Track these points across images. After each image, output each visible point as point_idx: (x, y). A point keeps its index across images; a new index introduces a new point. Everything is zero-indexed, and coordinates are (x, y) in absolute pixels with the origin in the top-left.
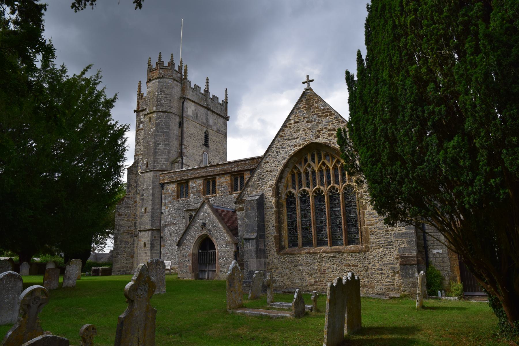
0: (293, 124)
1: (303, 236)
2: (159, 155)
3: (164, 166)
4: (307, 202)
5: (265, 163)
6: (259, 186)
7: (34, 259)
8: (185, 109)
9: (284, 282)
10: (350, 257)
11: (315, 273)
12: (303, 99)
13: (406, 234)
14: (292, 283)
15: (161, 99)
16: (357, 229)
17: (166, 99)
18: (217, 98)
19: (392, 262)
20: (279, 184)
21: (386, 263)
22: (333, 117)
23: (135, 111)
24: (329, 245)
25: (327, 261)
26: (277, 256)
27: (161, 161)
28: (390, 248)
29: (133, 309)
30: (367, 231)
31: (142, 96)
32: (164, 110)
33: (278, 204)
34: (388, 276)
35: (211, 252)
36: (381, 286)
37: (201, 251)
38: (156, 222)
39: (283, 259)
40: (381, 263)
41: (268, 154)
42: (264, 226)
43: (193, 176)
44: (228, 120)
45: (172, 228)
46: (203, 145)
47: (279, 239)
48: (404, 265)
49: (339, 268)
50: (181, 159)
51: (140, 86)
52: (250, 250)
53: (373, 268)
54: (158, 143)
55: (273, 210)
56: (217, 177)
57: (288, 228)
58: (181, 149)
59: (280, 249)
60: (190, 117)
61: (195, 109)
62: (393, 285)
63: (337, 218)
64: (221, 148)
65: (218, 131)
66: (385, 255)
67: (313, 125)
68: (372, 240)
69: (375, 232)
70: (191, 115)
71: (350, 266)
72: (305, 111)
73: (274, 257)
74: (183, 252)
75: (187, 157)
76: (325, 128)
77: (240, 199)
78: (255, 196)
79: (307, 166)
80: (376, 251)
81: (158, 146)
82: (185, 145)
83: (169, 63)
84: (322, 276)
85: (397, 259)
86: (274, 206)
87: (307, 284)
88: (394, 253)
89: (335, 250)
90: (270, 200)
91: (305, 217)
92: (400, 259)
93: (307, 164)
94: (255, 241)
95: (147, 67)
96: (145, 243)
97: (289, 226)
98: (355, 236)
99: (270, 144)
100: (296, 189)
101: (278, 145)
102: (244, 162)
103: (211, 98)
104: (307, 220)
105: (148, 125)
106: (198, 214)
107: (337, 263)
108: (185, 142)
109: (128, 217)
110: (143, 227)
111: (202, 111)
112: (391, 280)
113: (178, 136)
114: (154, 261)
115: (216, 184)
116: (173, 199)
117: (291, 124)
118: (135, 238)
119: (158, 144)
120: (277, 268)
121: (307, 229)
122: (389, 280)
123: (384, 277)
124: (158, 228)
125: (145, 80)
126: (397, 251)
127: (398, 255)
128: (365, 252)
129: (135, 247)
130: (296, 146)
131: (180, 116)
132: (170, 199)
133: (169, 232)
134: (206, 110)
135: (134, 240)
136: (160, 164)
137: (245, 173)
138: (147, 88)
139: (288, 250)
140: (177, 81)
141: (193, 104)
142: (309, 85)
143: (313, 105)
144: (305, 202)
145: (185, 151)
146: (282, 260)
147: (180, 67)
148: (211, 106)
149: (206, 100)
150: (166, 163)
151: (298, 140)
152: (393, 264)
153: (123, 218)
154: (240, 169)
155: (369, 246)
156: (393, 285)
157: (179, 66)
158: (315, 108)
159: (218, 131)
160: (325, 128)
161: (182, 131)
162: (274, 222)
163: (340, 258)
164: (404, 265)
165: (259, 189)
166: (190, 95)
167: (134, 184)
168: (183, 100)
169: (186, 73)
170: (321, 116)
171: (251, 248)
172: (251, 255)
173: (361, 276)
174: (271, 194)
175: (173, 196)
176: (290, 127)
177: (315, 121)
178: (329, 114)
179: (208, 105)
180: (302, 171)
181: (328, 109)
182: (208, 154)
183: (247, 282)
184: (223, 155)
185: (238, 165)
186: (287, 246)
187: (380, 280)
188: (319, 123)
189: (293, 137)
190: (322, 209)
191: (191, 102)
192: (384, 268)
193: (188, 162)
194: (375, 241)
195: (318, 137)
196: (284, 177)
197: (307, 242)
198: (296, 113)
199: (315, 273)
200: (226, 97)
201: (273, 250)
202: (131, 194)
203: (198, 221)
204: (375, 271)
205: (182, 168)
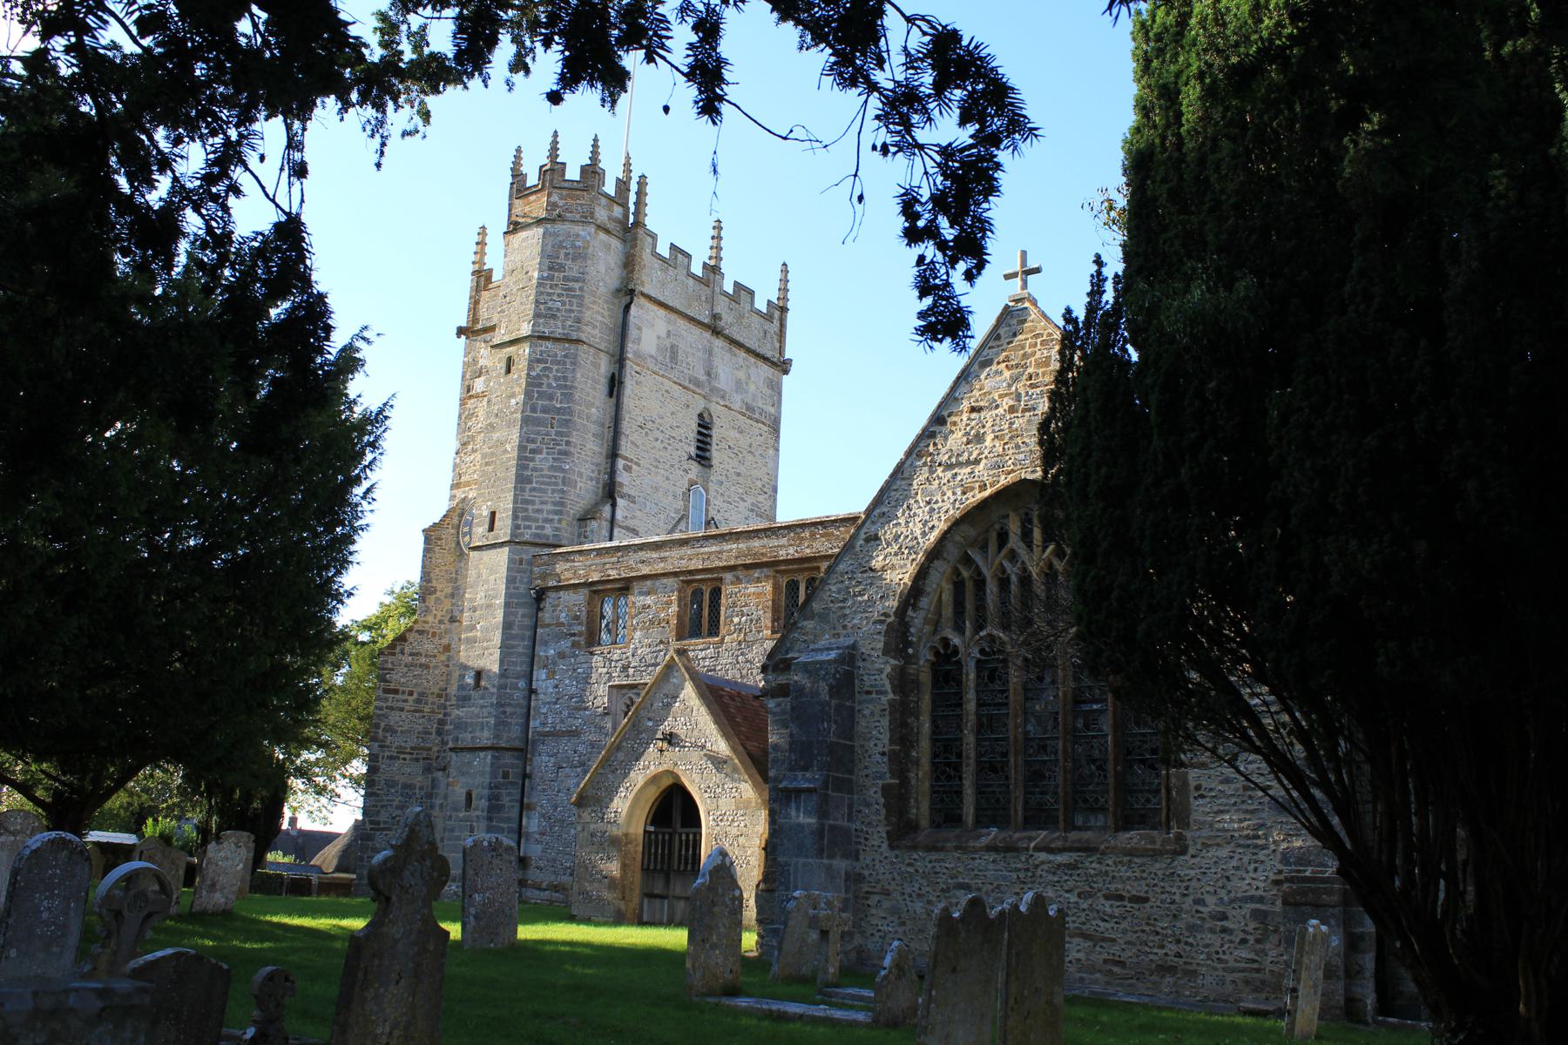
1: (980, 792)
2: (534, 489)
3: (548, 530)
4: (1000, 679)
8: (632, 332)
10: (1123, 869)
12: (1002, 331)
15: (549, 294)
16: (1158, 776)
17: (567, 296)
18: (751, 293)
19: (1260, 892)
20: (910, 613)
21: (1239, 895)
23: (461, 331)
24: (1061, 825)
25: (1051, 877)
27: (538, 511)
28: (1256, 846)
29: (387, 920)
31: (489, 279)
32: (559, 332)
33: (903, 682)
34: (1244, 941)
36: (1221, 973)
38: (513, 721)
39: (909, 865)
40: (1223, 893)
41: (877, 512)
42: (851, 749)
43: (646, 570)
44: (786, 372)
45: (565, 746)
46: (690, 458)
47: (897, 799)
48: (1297, 904)
49: (1085, 906)
50: (607, 508)
51: (481, 244)
53: (1197, 911)
54: (532, 446)
55: (884, 699)
56: (728, 576)
57: (933, 764)
58: (612, 473)
59: (902, 832)
60: (649, 360)
61: (669, 333)
62: (1258, 971)
63: (1093, 737)
64: (754, 473)
65: (749, 411)
66: (1237, 868)
69: (1211, 790)
70: (653, 353)
75: (631, 499)
78: (828, 649)
79: (1005, 557)
80: (1210, 855)
81: (533, 460)
82: (626, 458)
83: (584, 169)
86: (888, 687)
89: (1077, 845)
92: (1286, 886)
93: (1004, 552)
94: (815, 797)
95: (510, 180)
96: (469, 795)
97: (935, 755)
98: (1148, 801)
99: (886, 477)
100: (968, 633)
103: (726, 294)
104: (997, 739)
105: (500, 384)
108: (625, 448)
109: (418, 701)
110: (466, 738)
111: (693, 338)
112: (1252, 956)
113: (603, 425)
114: (485, 844)
115: (723, 601)
116: (574, 645)
118: (440, 774)
119: (533, 451)
120: (887, 893)
122: (1245, 954)
123: (1231, 942)
124: (517, 744)
125: (499, 224)
127: (1280, 872)
129: (437, 808)
131: (613, 356)
132: (565, 644)
133: (552, 760)
134: (707, 335)
135: (433, 780)
136: (536, 520)
138: (505, 256)
140: (607, 231)
141: (662, 312)
142: (1025, 285)
143: (1034, 354)
144: (992, 679)
145: (623, 477)
147: (623, 185)
148: (727, 319)
149: (711, 301)
150: (556, 517)
152: (1261, 900)
153: (400, 704)
154: (808, 551)
155: (1188, 834)
156: (1258, 971)
157: (618, 180)
158: (1038, 365)
159: (749, 411)
161: (618, 407)
162: (886, 738)
163: (1092, 872)
164: (1297, 904)
166: (650, 280)
167: (443, 588)
168: (628, 298)
169: (640, 203)
173: (1157, 933)
174: (881, 645)
175: (574, 635)
179: (716, 317)
180: (987, 573)
182: (707, 491)
184: (761, 498)
185: (802, 539)
186: (924, 823)
187: (1217, 953)
191: (655, 308)
192: (1234, 912)
193: (634, 517)
196: (928, 589)
197: (993, 814)
200: (784, 290)
201: (878, 837)
202: (430, 619)
204: (1203, 919)
205: (611, 540)
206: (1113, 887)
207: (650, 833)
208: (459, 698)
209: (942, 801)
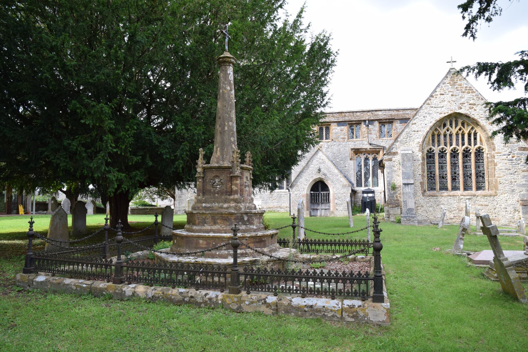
0: (439, 96)
5: (412, 124)
6: (407, 142)
7: (119, 193)
9: (428, 217)
11: (455, 210)
12: (448, 76)
13: (525, 185)
14: (435, 217)
22: (474, 94)
26: (423, 197)
30: (496, 182)
35: (324, 194)
37: (312, 192)
40: (506, 204)
52: (409, 193)
67: (457, 98)
68: (500, 188)
71: (482, 205)
72: (450, 87)
73: (420, 198)
74: (296, 193)
76: (467, 102)
77: (389, 151)
84: (460, 212)
85: (518, 201)
87: (447, 218)
88: (516, 198)
90: (417, 154)
91: (442, 168)
97: (428, 175)
101: (425, 110)
102: (331, 115)
106: (311, 161)
107: (472, 203)
117: (437, 95)
120: (422, 206)
121: (443, 178)
126: (518, 196)
128: (494, 196)
130: (442, 113)
137: (332, 124)
139: (428, 193)
143: (457, 82)
144: (442, 158)
146: (427, 200)
151: (443, 108)
152: (514, 205)
155: (497, 192)
158: (459, 85)
160: (467, 102)
165: (407, 145)
170: (464, 92)
171: (409, 191)
172: (409, 197)
176: (436, 97)
177: (459, 95)
178: (470, 91)
181: (470, 87)
183: (407, 216)
186: (427, 190)
188: (462, 97)
189: (439, 106)
190: (456, 164)
194: (502, 188)
195: (461, 108)
197: (444, 188)
198: (442, 87)
199: (455, 210)
203: (312, 166)
206: (480, 203)
207: (312, 193)
208: (466, 166)
209: (430, 185)
